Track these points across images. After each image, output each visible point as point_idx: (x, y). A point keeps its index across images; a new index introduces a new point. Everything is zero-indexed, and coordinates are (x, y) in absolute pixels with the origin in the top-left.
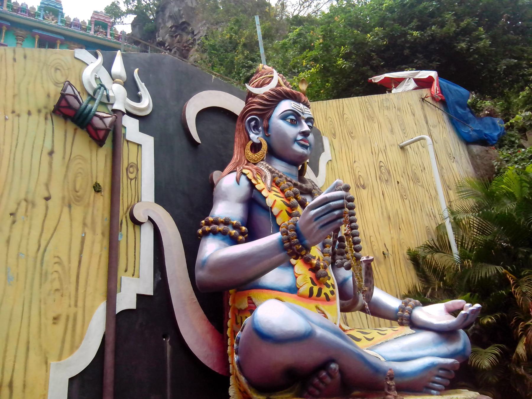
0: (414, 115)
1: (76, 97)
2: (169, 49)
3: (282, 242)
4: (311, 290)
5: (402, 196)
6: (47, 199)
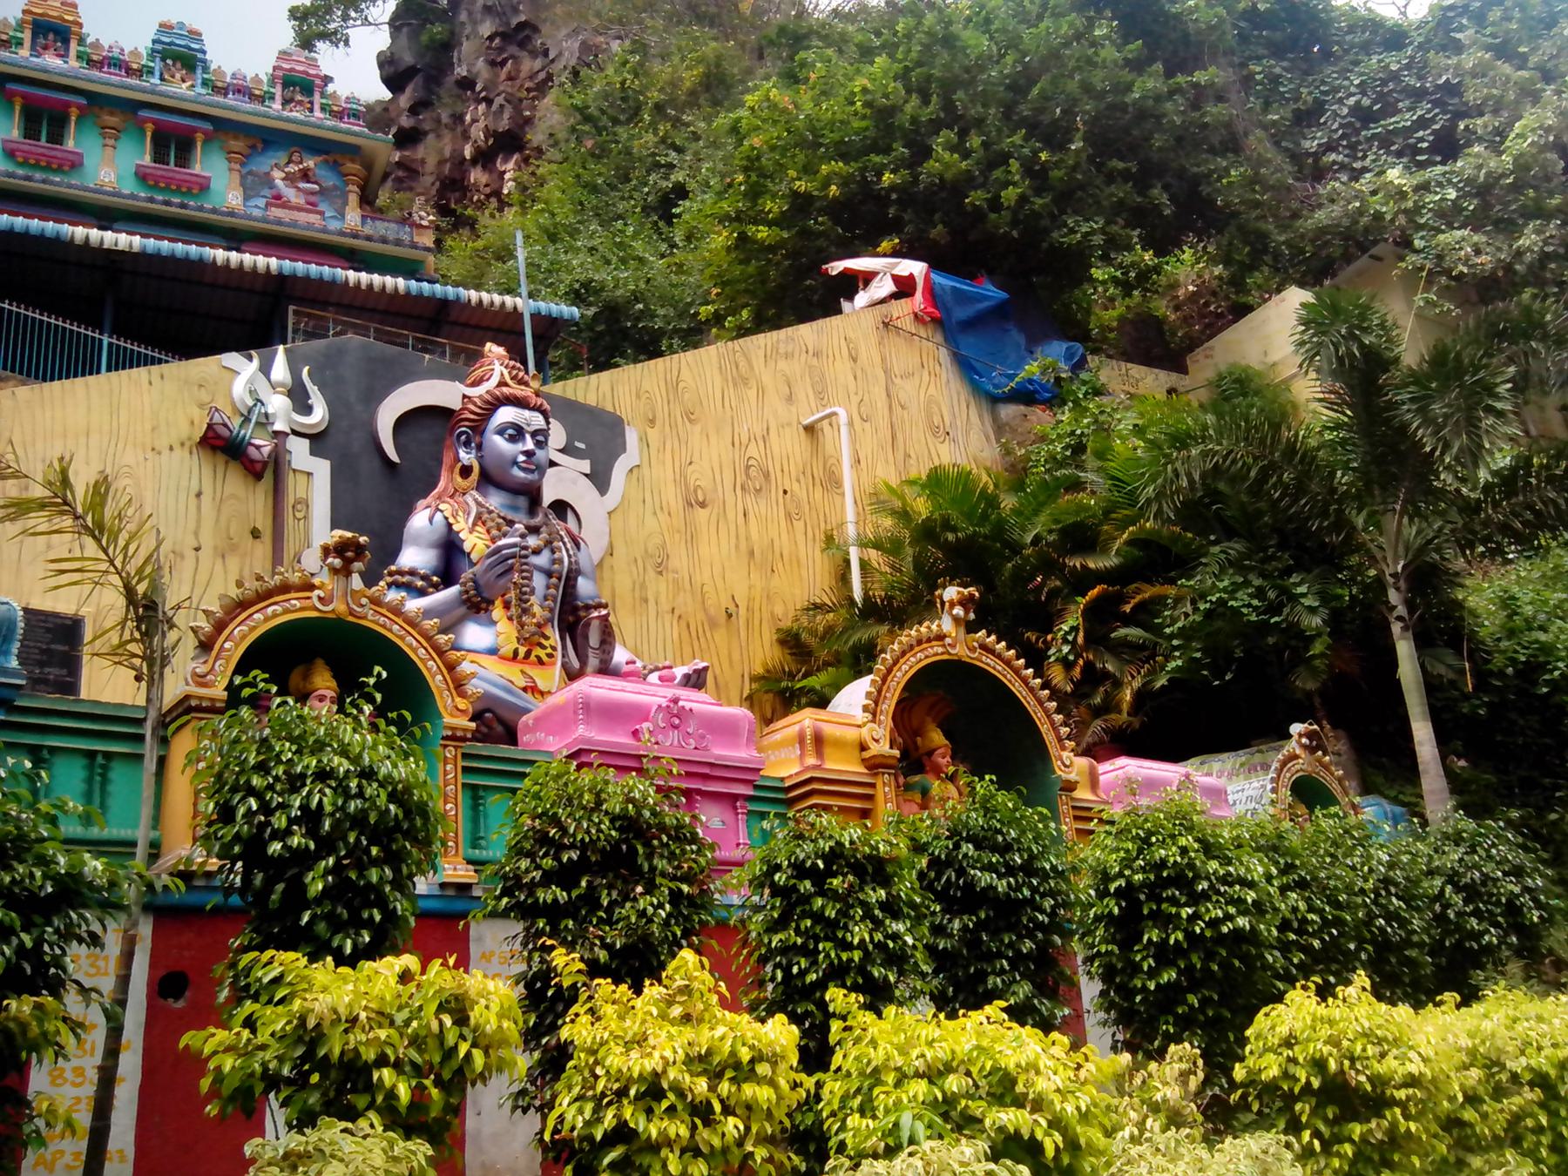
0: (855, 360)
1: (225, 425)
2: (484, 99)
3: (461, 593)
4: (516, 652)
5: (788, 516)
6: (197, 549)
